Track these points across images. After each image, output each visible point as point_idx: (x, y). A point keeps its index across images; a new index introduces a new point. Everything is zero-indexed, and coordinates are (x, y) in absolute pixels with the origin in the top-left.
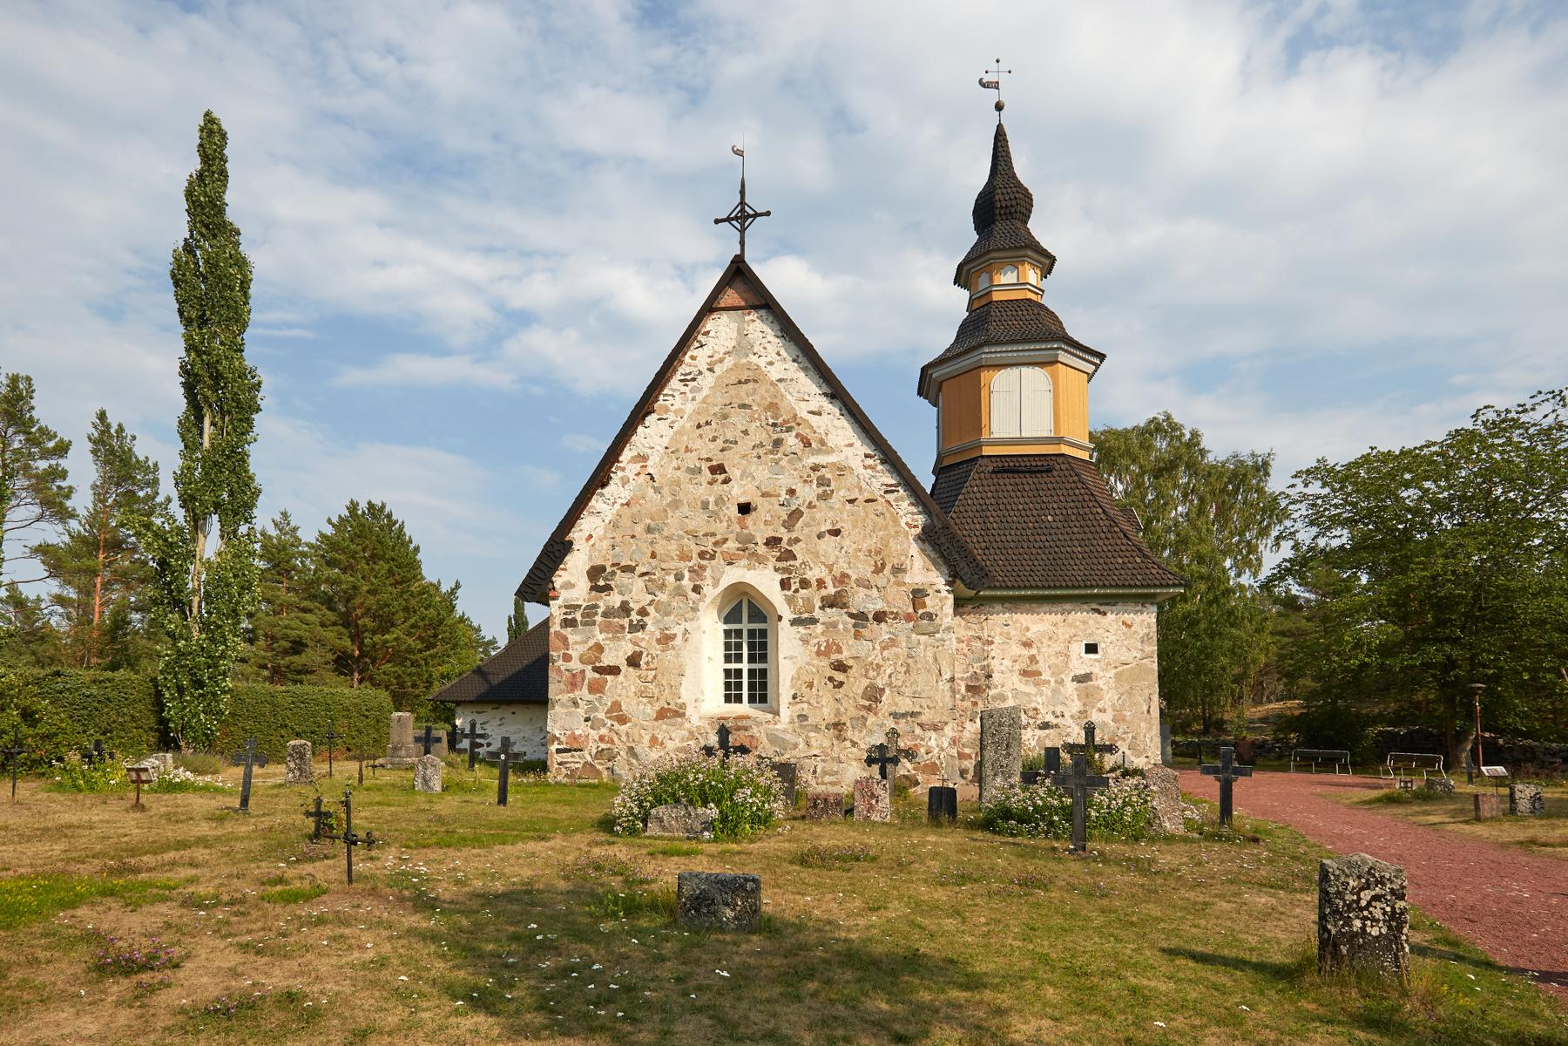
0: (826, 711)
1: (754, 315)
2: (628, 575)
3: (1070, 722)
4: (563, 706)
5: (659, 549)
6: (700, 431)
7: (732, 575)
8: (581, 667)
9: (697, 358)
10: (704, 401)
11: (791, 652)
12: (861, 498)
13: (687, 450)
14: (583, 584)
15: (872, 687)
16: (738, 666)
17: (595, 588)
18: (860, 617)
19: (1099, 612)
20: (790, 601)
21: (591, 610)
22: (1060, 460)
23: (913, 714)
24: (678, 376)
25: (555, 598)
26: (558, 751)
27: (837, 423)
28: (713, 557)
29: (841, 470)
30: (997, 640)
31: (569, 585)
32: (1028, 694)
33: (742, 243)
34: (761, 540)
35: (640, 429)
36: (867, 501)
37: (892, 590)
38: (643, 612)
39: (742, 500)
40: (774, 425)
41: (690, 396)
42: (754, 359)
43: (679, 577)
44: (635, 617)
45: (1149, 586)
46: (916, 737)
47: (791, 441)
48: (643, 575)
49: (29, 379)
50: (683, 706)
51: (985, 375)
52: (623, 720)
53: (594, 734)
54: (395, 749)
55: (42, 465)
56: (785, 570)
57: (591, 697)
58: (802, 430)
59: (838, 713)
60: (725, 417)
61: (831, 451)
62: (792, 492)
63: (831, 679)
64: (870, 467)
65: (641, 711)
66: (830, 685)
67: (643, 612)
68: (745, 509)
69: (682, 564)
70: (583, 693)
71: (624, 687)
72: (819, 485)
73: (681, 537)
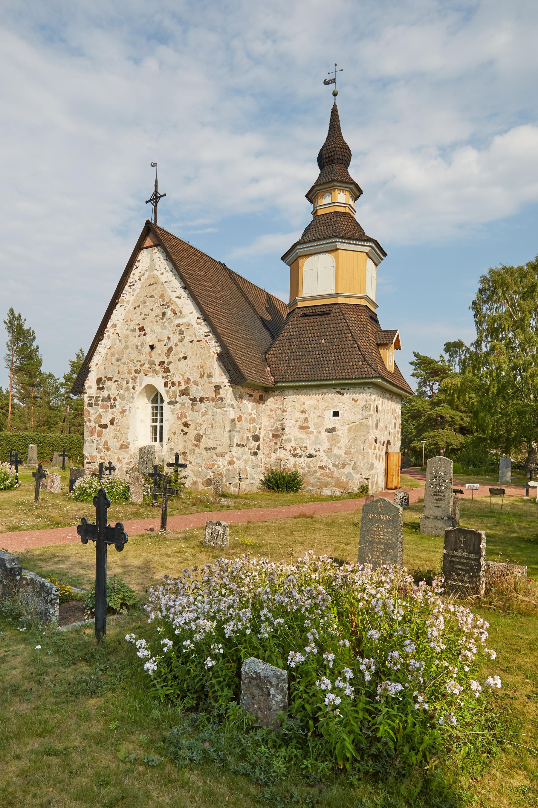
0: (180, 446)
1: (156, 250)
2: (110, 381)
4: (89, 442)
6: (135, 311)
7: (149, 380)
9: (135, 274)
10: (137, 296)
12: (196, 340)
13: (131, 320)
14: (95, 386)
15: (198, 435)
16: (156, 424)
17: (100, 389)
18: (194, 400)
19: (339, 393)
20: (167, 392)
22: (336, 307)
23: (214, 449)
24: (128, 284)
25: (85, 393)
26: (88, 463)
29: (188, 325)
30: (289, 410)
31: (90, 387)
32: (302, 439)
33: (156, 213)
35: (114, 311)
36: (198, 341)
37: (207, 386)
39: (151, 344)
40: (163, 305)
41: (132, 293)
42: (155, 272)
43: (128, 382)
44: (112, 401)
45: (369, 378)
46: (214, 460)
47: (169, 313)
50: (128, 443)
51: (301, 261)
52: (108, 449)
53: (99, 456)
54: (30, 460)
56: (166, 377)
58: (172, 307)
59: (185, 448)
60: (145, 302)
61: (183, 317)
62: (169, 338)
63: (182, 431)
65: (114, 444)
66: (182, 434)
68: (152, 347)
70: (95, 437)
71: (109, 432)
72: (180, 334)
73: (128, 363)
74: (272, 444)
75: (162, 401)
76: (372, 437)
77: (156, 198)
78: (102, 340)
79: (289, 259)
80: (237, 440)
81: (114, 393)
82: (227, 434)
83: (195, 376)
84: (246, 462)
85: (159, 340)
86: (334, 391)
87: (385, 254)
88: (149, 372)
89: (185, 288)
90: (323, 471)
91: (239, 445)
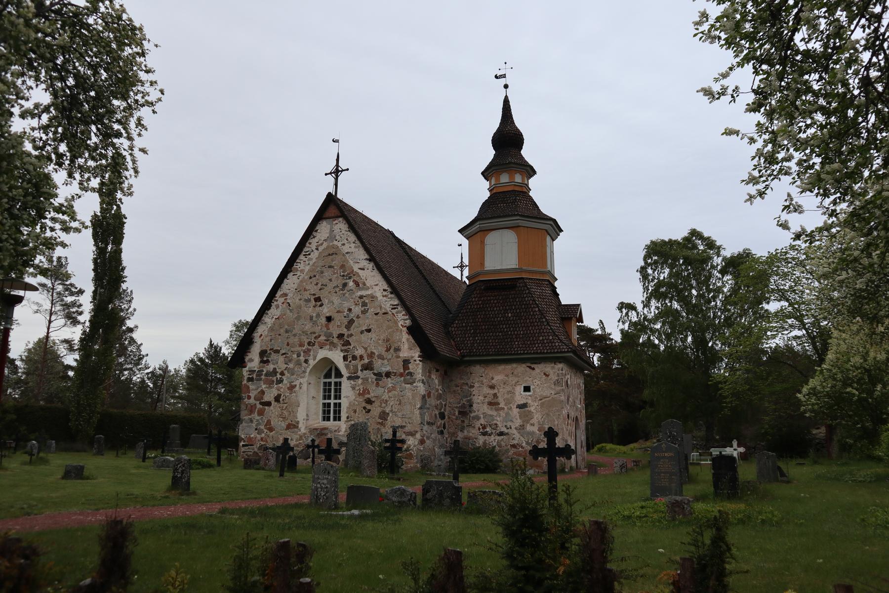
3: (515, 432)
5: (291, 341)
7: (322, 354)
8: (255, 402)
9: (313, 242)
10: (313, 265)
11: (348, 393)
12: (381, 312)
14: (257, 359)
17: (262, 362)
18: (379, 375)
19: (530, 367)
20: (347, 367)
21: (260, 372)
26: (243, 446)
27: (372, 274)
28: (314, 345)
30: (476, 385)
31: (251, 360)
33: (336, 185)
34: (335, 336)
38: (282, 374)
39: (328, 315)
43: (299, 355)
44: (279, 376)
47: (351, 284)
48: (283, 354)
49: (66, 258)
50: (298, 422)
52: (271, 429)
53: (259, 437)
55: (69, 299)
57: (258, 418)
58: (355, 278)
60: (322, 272)
61: (368, 289)
62: (350, 310)
63: (365, 408)
64: (385, 296)
67: (282, 374)
68: (329, 319)
69: (300, 349)
70: (255, 416)
71: (273, 412)
74: (459, 422)
75: (339, 374)
76: (565, 412)
77: (337, 172)
78: (269, 309)
79: (468, 232)
80: (427, 418)
81: (281, 365)
82: (417, 412)
83: (379, 350)
84: (434, 440)
85: (338, 312)
86: (524, 365)
87: (561, 231)
88: (326, 345)
89: (371, 259)
90: (515, 450)
91: (428, 423)
